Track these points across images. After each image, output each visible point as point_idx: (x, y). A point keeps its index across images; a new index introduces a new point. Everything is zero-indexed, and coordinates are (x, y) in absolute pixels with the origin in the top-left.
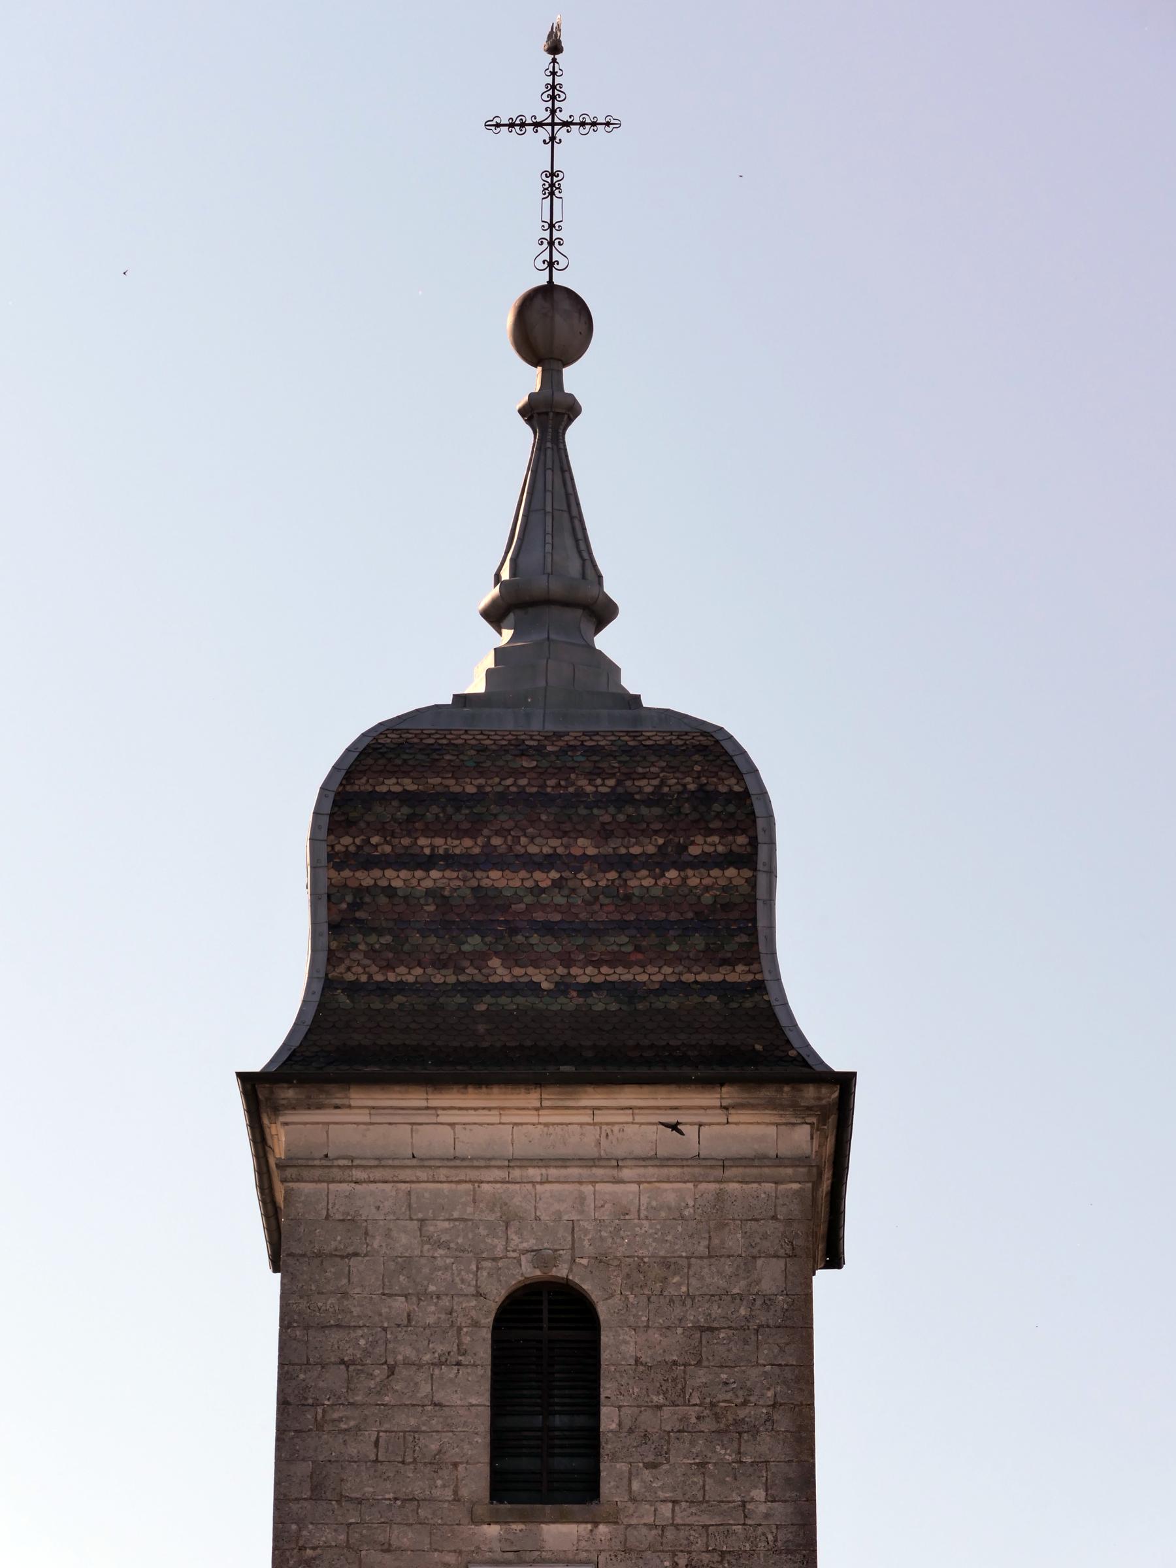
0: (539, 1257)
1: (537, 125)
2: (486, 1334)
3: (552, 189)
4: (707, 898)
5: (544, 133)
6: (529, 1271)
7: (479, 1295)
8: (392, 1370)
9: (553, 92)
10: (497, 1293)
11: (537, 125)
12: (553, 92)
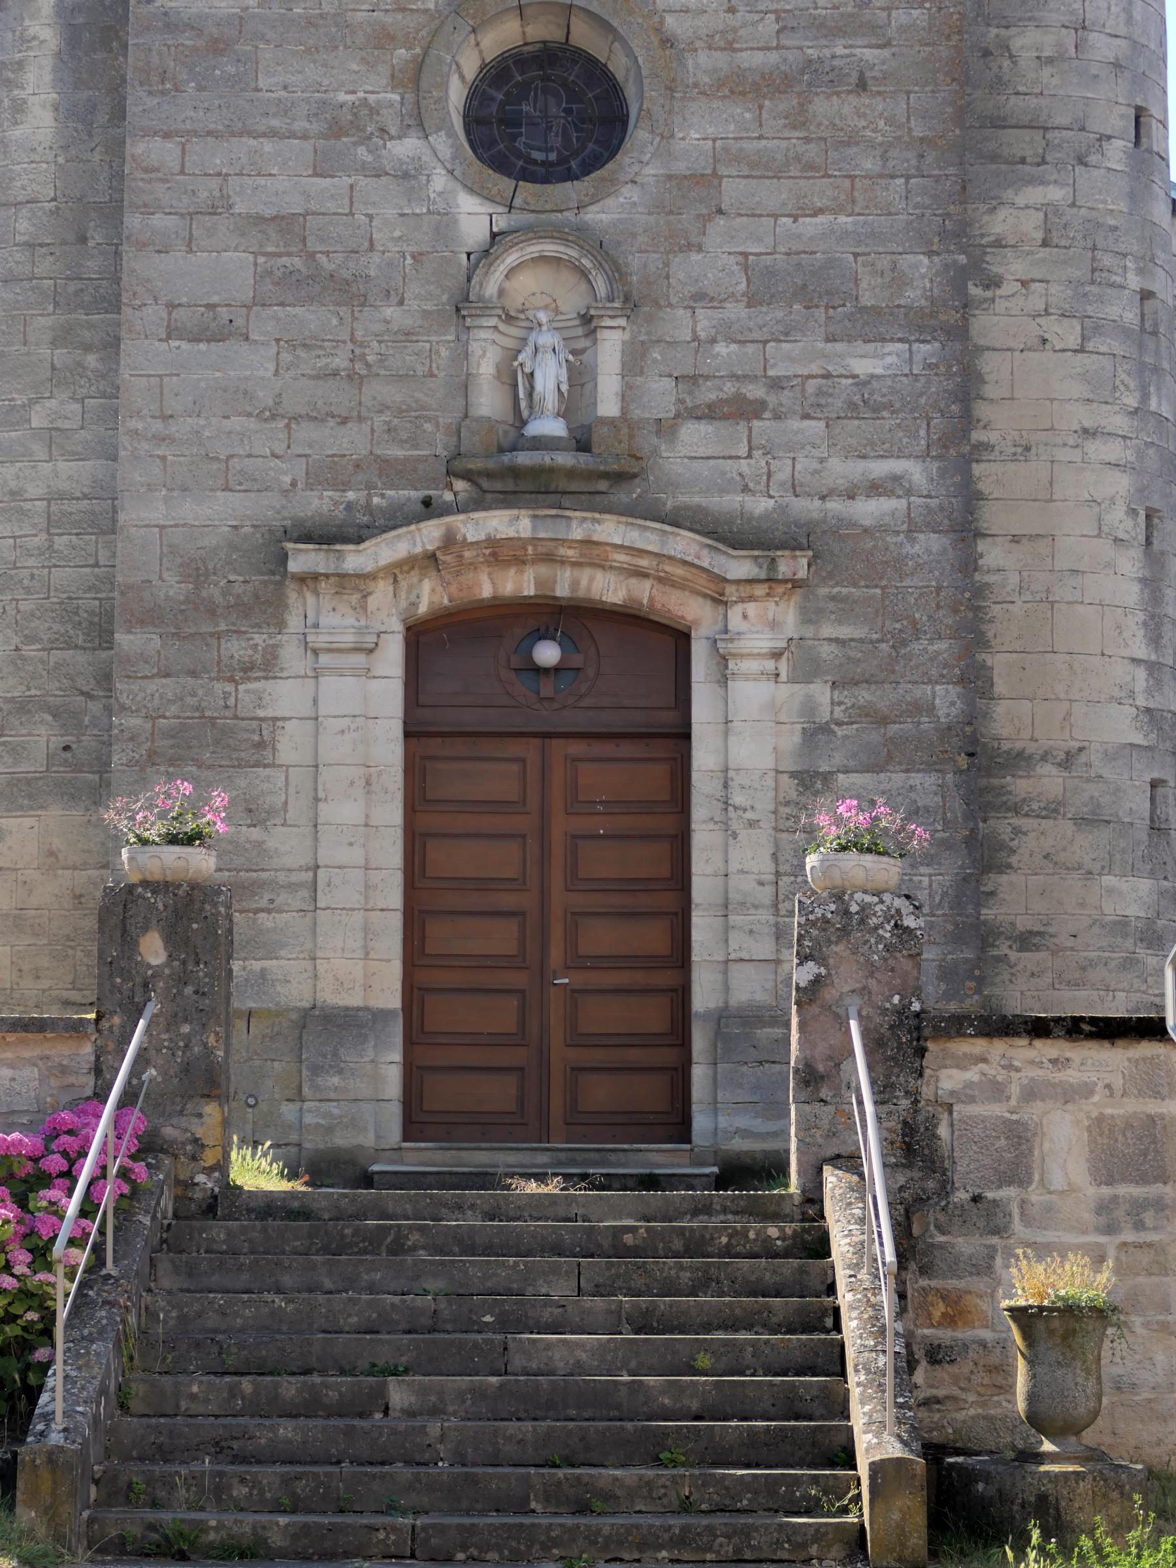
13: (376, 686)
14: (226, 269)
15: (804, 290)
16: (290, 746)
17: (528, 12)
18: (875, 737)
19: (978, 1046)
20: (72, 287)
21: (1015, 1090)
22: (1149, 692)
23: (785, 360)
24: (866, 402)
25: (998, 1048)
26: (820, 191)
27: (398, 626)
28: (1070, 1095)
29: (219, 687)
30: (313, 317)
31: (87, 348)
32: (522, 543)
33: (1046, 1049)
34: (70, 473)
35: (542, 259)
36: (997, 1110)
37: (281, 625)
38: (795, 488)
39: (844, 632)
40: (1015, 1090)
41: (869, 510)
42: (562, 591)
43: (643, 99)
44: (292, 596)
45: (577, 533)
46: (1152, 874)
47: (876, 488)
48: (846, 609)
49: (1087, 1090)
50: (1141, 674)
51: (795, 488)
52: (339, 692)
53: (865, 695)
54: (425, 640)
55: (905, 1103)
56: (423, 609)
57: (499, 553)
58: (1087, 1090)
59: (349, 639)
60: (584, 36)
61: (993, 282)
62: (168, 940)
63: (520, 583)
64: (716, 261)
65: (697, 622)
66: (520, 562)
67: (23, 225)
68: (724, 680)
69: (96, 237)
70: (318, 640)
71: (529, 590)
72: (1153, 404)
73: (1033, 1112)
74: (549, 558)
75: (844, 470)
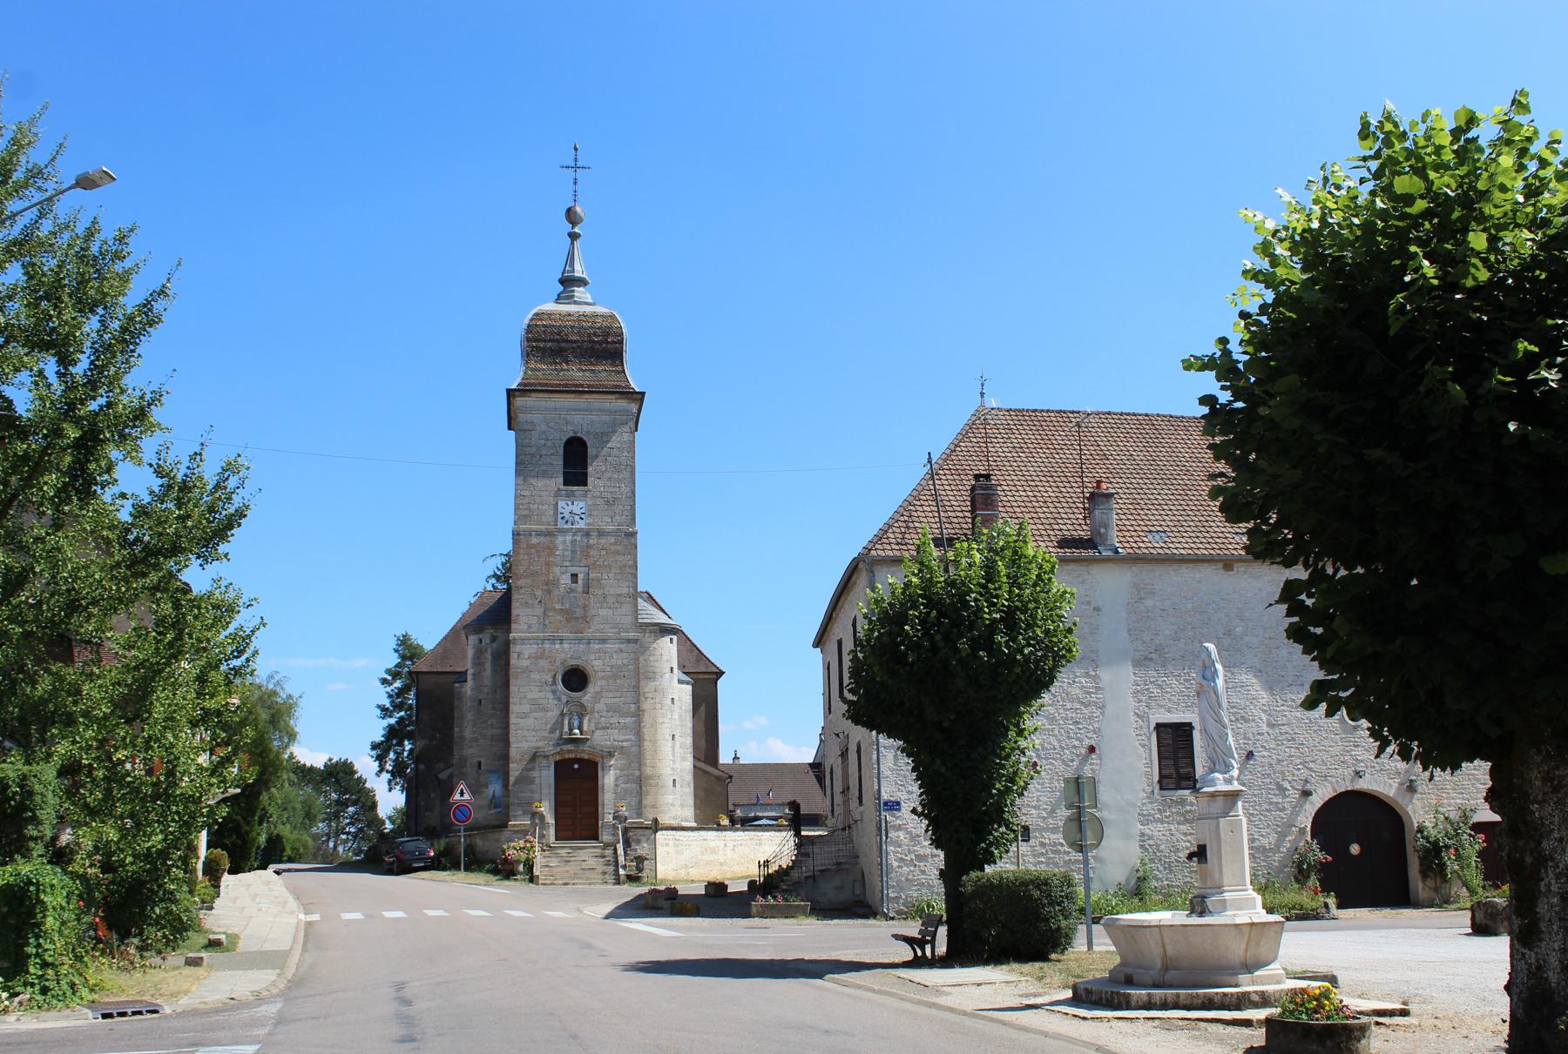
14: (526, 708)
16: (537, 781)
24: (625, 727)
52: (545, 773)
54: (556, 763)
57: (569, 751)
64: (600, 706)
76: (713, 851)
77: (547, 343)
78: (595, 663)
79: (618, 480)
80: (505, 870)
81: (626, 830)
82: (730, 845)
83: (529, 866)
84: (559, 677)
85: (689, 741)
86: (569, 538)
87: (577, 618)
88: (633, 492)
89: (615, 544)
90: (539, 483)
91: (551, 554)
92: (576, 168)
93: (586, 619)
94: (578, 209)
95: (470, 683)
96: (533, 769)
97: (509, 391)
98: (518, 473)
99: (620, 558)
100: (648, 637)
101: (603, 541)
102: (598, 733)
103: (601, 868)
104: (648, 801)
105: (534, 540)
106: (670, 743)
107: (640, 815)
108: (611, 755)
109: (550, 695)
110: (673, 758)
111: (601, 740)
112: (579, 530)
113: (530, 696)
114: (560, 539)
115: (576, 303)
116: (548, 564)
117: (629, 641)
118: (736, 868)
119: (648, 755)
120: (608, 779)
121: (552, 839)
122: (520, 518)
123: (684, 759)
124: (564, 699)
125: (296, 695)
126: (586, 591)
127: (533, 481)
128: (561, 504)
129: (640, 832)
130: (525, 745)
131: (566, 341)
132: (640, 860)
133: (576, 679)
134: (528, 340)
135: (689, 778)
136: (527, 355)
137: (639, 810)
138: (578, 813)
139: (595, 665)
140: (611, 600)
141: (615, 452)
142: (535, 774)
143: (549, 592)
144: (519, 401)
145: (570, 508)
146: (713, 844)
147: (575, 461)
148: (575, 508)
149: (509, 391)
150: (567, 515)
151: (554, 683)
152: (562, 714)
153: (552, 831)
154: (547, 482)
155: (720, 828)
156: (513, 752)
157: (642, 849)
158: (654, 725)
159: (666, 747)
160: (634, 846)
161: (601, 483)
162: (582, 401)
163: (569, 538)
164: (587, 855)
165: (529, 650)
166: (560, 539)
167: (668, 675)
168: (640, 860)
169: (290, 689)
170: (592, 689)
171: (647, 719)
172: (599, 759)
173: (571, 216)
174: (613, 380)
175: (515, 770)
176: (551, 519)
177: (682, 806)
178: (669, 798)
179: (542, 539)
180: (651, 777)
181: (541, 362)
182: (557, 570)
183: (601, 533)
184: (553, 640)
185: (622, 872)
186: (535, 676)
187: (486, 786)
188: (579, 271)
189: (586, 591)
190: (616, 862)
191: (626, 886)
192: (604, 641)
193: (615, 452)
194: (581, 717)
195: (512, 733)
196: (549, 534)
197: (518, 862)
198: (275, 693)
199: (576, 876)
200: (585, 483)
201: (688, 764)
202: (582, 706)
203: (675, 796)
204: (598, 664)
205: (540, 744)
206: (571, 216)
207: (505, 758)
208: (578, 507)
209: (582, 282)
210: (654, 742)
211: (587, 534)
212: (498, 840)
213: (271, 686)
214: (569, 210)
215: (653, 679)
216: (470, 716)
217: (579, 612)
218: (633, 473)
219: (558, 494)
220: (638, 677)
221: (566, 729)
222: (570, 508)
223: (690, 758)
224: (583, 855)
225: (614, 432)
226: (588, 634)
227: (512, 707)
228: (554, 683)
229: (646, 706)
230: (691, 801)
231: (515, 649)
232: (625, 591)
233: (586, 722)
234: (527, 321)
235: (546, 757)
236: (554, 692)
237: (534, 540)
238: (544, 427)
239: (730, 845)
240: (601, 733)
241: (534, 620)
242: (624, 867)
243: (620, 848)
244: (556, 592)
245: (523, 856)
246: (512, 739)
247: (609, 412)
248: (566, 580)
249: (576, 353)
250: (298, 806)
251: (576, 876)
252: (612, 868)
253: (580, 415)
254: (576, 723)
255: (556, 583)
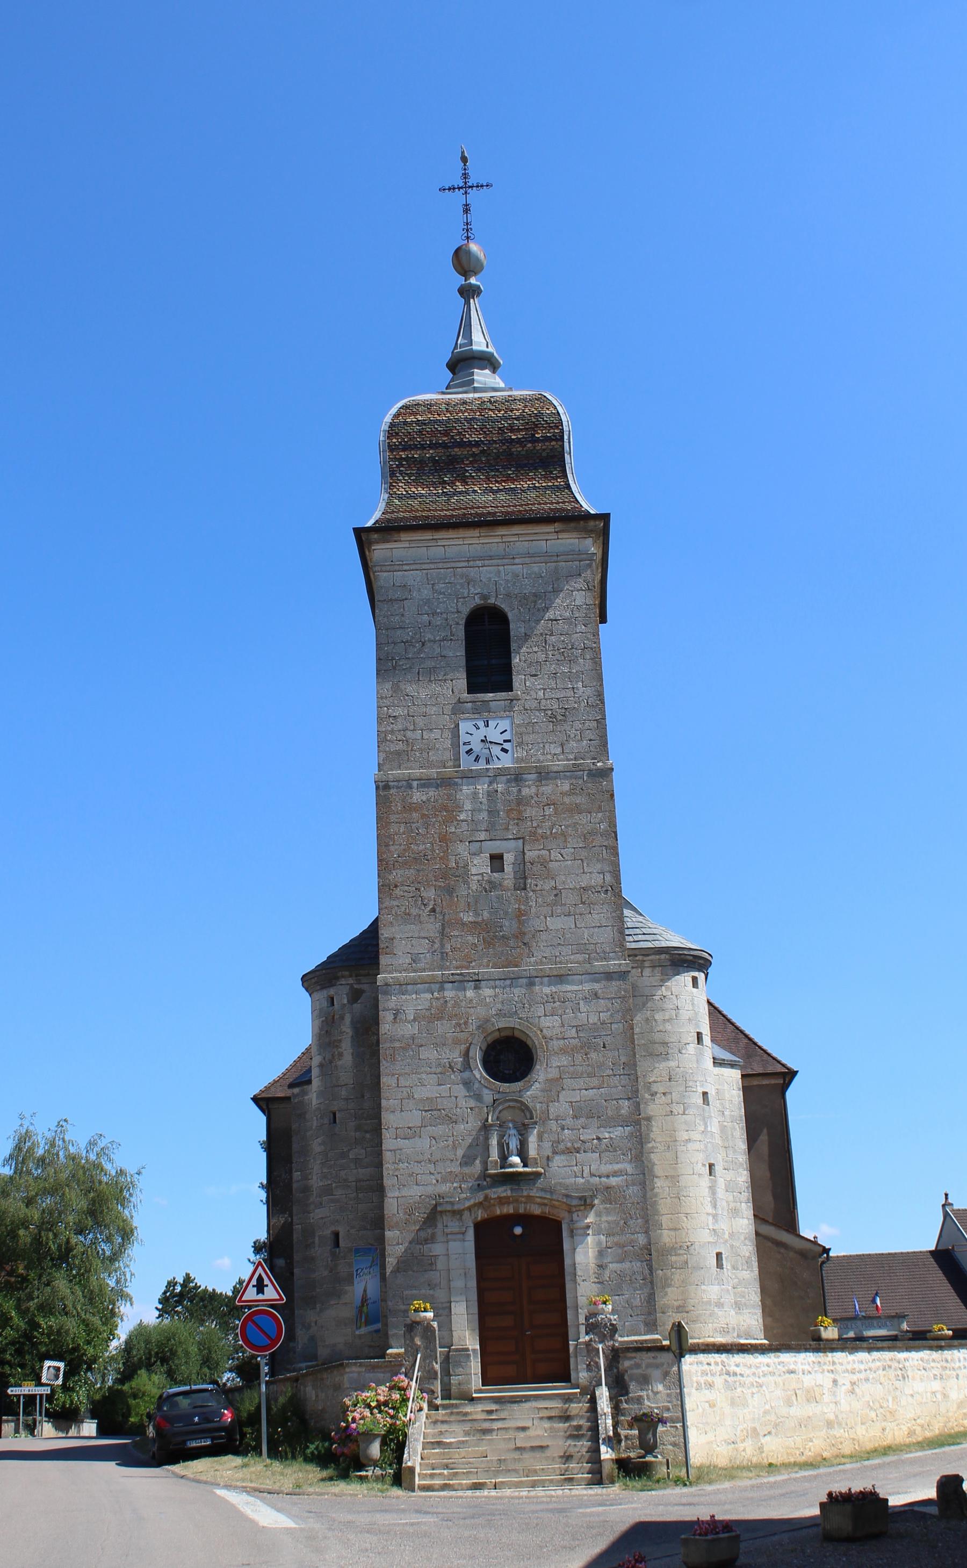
0: (484, 597)
1: (459, 188)
2: (462, 627)
3: (467, 209)
4: (544, 454)
5: (462, 191)
6: (478, 601)
7: (458, 612)
8: (423, 645)
9: (465, 176)
10: (466, 611)
11: (459, 188)
12: (465, 176)
13: (466, 1243)
14: (414, 1117)
15: (587, 1112)
16: (440, 1265)
17: (497, 862)
18: (620, 1251)
19: (633, 1355)
20: (360, 1112)
21: (644, 1366)
22: (713, 1224)
23: (588, 1135)
24: (612, 1147)
25: (638, 1355)
26: (595, 1082)
27: (472, 1225)
28: (657, 1366)
29: (418, 1247)
30: (440, 1130)
31: (366, 1132)
32: (508, 1197)
33: (651, 1354)
34: (363, 1172)
35: (509, 1107)
36: (639, 1371)
37: (436, 1226)
38: (592, 1175)
39: (610, 1218)
40: (644, 1366)
41: (614, 1181)
42: (521, 1211)
43: (540, 1054)
44: (439, 1217)
45: (525, 1193)
46: (719, 1284)
47: (615, 1174)
48: (608, 1212)
49: (662, 1364)
50: (710, 1218)
51: (592, 1175)
52: (455, 1246)
53: (616, 1239)
54: (480, 1228)
55: (615, 1370)
56: (479, 1218)
57: (502, 1201)
58: (662, 1364)
59: (457, 1230)
60: (517, 1034)
61: (654, 1094)
62: (422, 1338)
63: (509, 1209)
64: (560, 1107)
65: (563, 1218)
66: (509, 1203)
67: (344, 1093)
68: (572, 1237)
69: (367, 1095)
70: (448, 1230)
71: (511, 1211)
72: (709, 1129)
73: (649, 1371)
74: (517, 1201)
75: (606, 1168)
76: (812, 1397)
77: (425, 451)
78: (546, 1022)
79: (570, 677)
80: (343, 1459)
81: (615, 1356)
82: (845, 1380)
83: (396, 1442)
84: (477, 1056)
85: (743, 1177)
86: (482, 787)
87: (505, 938)
88: (600, 695)
89: (571, 792)
90: (420, 691)
91: (451, 818)
92: (466, 187)
93: (522, 939)
94: (474, 247)
95: (316, 1083)
96: (432, 1239)
97: (360, 533)
98: (382, 673)
99: (583, 819)
100: (648, 977)
101: (547, 789)
102: (558, 1160)
103: (559, 1445)
104: (669, 1298)
105: (418, 796)
106: (705, 1181)
107: (652, 1326)
108: (586, 1204)
109: (460, 1090)
110: (712, 1210)
111: (564, 1174)
112: (501, 772)
113: (421, 1093)
114: (466, 790)
115: (476, 390)
116: (444, 839)
117: (609, 976)
118: (861, 1431)
119: (664, 1206)
120: (585, 1254)
121: (476, 1381)
122: (389, 758)
123: (735, 1212)
124: (488, 1097)
125: (131, 1169)
126: (522, 883)
127: (410, 689)
128: (465, 726)
129: (646, 1358)
130: (414, 1192)
131: (461, 444)
132: (647, 1423)
133: (509, 1056)
134: (391, 448)
135: (748, 1249)
136: (392, 474)
137: (650, 1315)
138: (528, 1332)
139: (547, 1026)
140: (569, 898)
141: (561, 626)
142: (437, 1249)
143: (450, 891)
144: (379, 551)
145: (483, 731)
146: (808, 1381)
147: (488, 649)
148: (490, 733)
149: (360, 533)
150: (477, 746)
151: (467, 1066)
152: (486, 1128)
153: (475, 1366)
154: (435, 688)
155: (818, 1344)
156: (392, 1206)
157: (654, 1398)
158: (672, 1144)
159: (698, 1188)
160: (634, 1390)
161: (537, 683)
162: (494, 541)
163: (482, 787)
164: (533, 1414)
165: (415, 1003)
166: (466, 790)
167: (692, 1048)
168: (647, 1423)
169: (121, 1160)
170: (541, 1074)
171: (657, 1134)
172: (563, 1215)
173: (464, 263)
174: (551, 502)
175: (396, 1243)
176: (448, 755)
177: (738, 1306)
178: (711, 1291)
179: (432, 793)
180: (673, 1250)
181: (417, 483)
182: (462, 849)
183: (544, 775)
184: (460, 982)
185: (606, 1453)
186: (429, 1054)
187: (350, 1280)
188: (480, 342)
189: (522, 883)
190: (595, 1429)
191: (615, 1490)
192: (560, 978)
193: (561, 626)
194: (523, 1131)
195: (388, 1168)
196: (445, 782)
197: (369, 1436)
198: (98, 1167)
199: (501, 1466)
200: (507, 686)
201: (745, 1223)
202: (525, 1109)
203: (724, 1292)
204: (550, 1024)
205: (444, 1188)
206: (464, 263)
207: (378, 1222)
208: (497, 730)
209: (487, 361)
210: (674, 1179)
211: (517, 777)
212: (338, 1388)
213: (92, 1157)
214: (457, 252)
215: (666, 1056)
216: (316, 1146)
217: (509, 926)
218: (597, 661)
219: (458, 709)
220: (632, 1052)
221: (494, 1155)
222: (483, 731)
223: (747, 1211)
224: (521, 1415)
225: (556, 591)
226: (529, 966)
227: (388, 1118)
228: (467, 1066)
229: (654, 1108)
230: (754, 1296)
231: (389, 1003)
232: (596, 880)
233: (532, 1140)
234: (388, 419)
235: (457, 1214)
236: (467, 1084)
237: (418, 796)
238: (426, 592)
239: (845, 1380)
240: (565, 1160)
241: (422, 947)
242: (613, 1442)
243: (603, 1394)
244: (462, 891)
245: (382, 1421)
246: (387, 1182)
247: (548, 557)
248: (480, 866)
249: (481, 468)
250: (193, 1349)
251: (501, 1466)
252: (585, 1444)
253: (489, 566)
254: (514, 1144)
255: (462, 873)
